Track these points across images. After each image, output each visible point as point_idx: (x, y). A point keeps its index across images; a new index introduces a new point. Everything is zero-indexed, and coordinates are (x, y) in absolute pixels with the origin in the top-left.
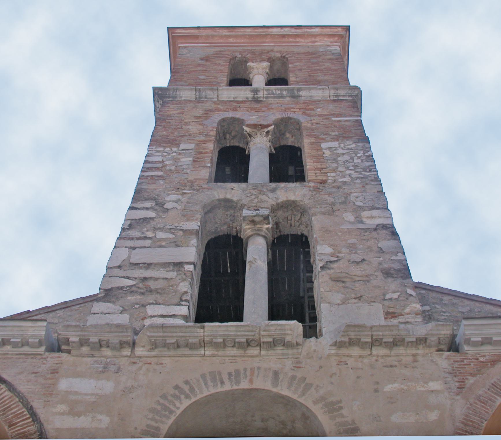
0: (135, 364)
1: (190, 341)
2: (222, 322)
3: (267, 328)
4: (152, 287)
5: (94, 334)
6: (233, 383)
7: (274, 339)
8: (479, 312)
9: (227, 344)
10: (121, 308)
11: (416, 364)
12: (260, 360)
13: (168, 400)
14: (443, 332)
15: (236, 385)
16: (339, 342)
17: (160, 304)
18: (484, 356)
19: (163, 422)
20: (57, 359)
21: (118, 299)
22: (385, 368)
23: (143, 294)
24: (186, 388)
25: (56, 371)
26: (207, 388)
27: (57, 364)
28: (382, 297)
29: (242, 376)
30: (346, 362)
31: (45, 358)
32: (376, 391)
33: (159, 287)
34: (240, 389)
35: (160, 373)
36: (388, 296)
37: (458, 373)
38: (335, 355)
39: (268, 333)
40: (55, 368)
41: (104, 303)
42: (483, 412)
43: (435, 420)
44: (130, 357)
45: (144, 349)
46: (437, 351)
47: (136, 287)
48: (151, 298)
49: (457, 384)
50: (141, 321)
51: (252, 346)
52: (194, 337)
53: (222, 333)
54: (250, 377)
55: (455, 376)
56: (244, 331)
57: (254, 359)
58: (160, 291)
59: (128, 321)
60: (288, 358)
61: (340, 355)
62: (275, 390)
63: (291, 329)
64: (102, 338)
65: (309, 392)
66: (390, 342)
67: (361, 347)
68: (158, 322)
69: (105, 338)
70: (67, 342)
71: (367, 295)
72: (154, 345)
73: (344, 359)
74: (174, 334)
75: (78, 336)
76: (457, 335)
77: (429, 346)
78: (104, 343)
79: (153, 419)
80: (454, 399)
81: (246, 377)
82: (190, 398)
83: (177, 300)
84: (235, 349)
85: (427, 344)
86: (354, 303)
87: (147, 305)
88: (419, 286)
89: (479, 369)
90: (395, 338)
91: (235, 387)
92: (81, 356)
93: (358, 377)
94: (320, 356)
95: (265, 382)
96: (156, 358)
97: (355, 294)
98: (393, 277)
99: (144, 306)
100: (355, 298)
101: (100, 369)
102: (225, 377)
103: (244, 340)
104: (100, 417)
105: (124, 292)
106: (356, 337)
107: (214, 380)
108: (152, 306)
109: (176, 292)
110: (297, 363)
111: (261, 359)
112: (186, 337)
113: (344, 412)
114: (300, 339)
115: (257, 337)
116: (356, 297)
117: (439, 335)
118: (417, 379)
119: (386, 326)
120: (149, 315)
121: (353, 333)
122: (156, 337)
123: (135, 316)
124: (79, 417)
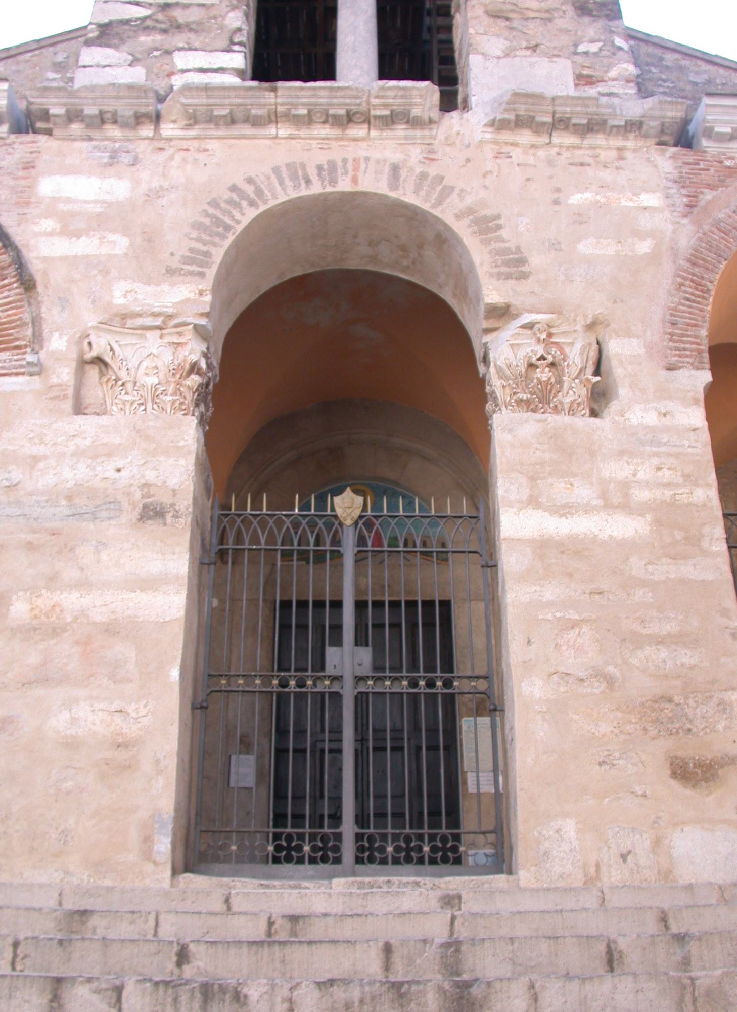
0: (162, 151)
1: (253, 112)
2: (305, 81)
3: (381, 93)
4: (181, 20)
5: (90, 101)
6: (326, 182)
7: (392, 111)
8: (723, 84)
9: (314, 118)
10: (130, 58)
11: (621, 163)
12: (368, 146)
13: (221, 209)
14: (670, 114)
15: (330, 185)
16: (500, 120)
17: (196, 50)
18: (732, 158)
19: (215, 245)
20: (31, 145)
21: (123, 41)
22: (570, 166)
23: (165, 31)
24: (250, 190)
25: (31, 165)
26: (284, 189)
27: (31, 153)
28: (572, 49)
29: (340, 171)
30: (509, 153)
31: (10, 145)
32: (556, 202)
33: (191, 19)
34: (338, 192)
35: (205, 165)
36: (581, 48)
37: (688, 182)
38: (493, 142)
39: (383, 100)
40: (30, 160)
41: (99, 49)
42: (722, 246)
43: (647, 253)
44: (152, 139)
45: (176, 127)
46: (659, 144)
47: (153, 20)
48: (179, 40)
49: (685, 200)
50: (166, 80)
51: (356, 123)
52: (260, 105)
53: (307, 100)
54: (353, 173)
55: (684, 187)
56: (343, 97)
57: (360, 143)
58: (193, 26)
59: (144, 79)
60: (414, 143)
61: (500, 142)
62: (393, 195)
63: (421, 96)
64: (105, 108)
65: (448, 200)
66: (584, 125)
67: (535, 129)
68: (196, 81)
69: (110, 109)
70: (45, 116)
71: (548, 44)
72: (193, 120)
73: (506, 149)
74: (227, 101)
75: (64, 105)
76: (691, 120)
77: (646, 136)
78: (108, 116)
79: (198, 240)
80: (678, 223)
81: (346, 173)
82: (257, 207)
83: (224, 43)
84: (327, 126)
85: (643, 132)
86: (525, 56)
87: (174, 51)
88: (632, 35)
89: (722, 178)
90: (592, 119)
91: (329, 189)
92: (69, 139)
93: (528, 180)
94: (467, 142)
95: (378, 181)
96: (197, 141)
97: (528, 41)
98: (592, 16)
99: (169, 52)
100: (527, 48)
101: (105, 160)
102: (313, 173)
103: (342, 112)
104: (112, 237)
105: (132, 28)
106: (527, 113)
107: (294, 177)
108: (182, 53)
109: (222, 28)
110: (429, 152)
111: (370, 143)
112: (246, 105)
113: (504, 233)
114: (435, 113)
115: (364, 108)
116: (529, 45)
117: (664, 118)
118: (623, 186)
119: (579, 98)
120: (180, 68)
121: (523, 107)
122: (197, 105)
123: (156, 71)
124: (79, 237)
